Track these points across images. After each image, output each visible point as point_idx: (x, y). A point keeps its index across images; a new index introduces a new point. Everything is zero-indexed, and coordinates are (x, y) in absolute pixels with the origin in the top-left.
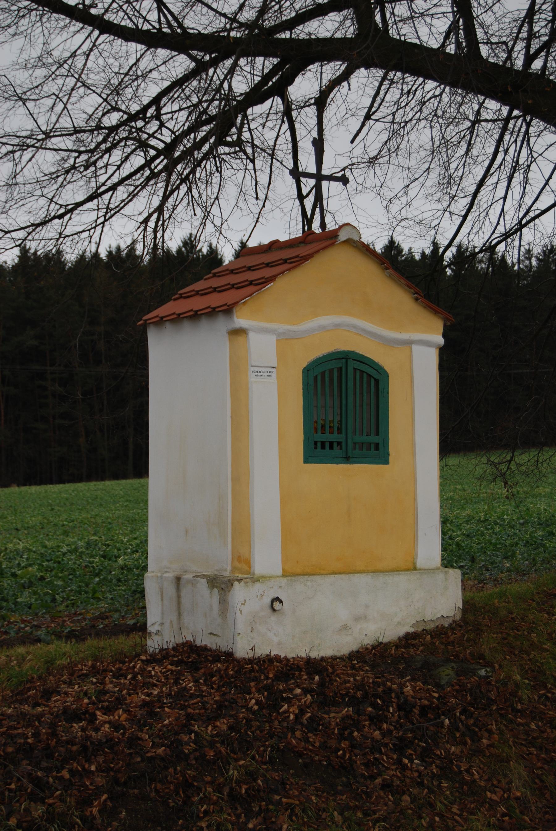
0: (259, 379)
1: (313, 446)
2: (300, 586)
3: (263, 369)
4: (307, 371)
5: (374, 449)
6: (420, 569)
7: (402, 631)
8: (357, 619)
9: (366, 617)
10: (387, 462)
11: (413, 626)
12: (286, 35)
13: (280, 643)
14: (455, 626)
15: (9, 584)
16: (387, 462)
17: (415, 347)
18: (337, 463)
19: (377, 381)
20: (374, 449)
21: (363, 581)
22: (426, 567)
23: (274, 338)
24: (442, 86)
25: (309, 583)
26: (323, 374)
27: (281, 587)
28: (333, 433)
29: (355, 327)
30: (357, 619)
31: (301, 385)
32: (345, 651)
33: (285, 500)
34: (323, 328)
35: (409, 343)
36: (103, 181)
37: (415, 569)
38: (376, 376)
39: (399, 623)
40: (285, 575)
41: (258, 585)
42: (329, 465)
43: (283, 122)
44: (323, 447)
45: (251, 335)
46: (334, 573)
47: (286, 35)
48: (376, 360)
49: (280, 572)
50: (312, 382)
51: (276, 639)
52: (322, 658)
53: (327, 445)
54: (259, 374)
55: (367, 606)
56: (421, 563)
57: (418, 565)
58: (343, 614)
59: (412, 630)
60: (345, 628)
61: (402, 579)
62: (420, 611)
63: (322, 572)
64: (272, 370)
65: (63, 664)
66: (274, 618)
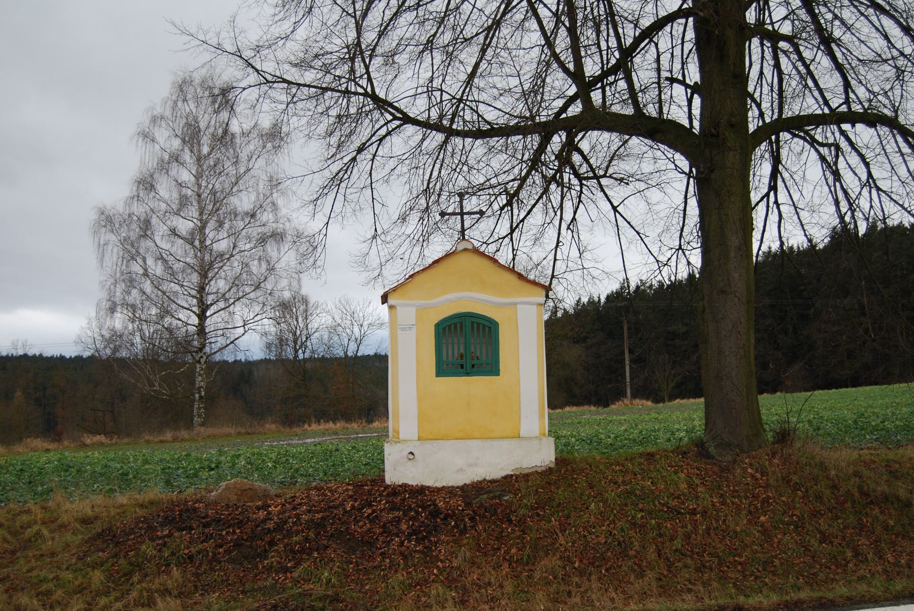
4: (437, 326)
5: (491, 367)
7: (504, 473)
8: (470, 465)
12: (564, 116)
14: (549, 471)
15: (410, 541)
19: (490, 328)
20: (491, 367)
23: (414, 309)
24: (768, 120)
26: (455, 325)
30: (470, 465)
32: (461, 484)
33: (420, 399)
35: (516, 304)
38: (488, 324)
41: (398, 445)
43: (894, 136)
45: (398, 308)
47: (564, 116)
50: (441, 331)
54: (403, 329)
57: (521, 435)
61: (505, 443)
66: (410, 463)
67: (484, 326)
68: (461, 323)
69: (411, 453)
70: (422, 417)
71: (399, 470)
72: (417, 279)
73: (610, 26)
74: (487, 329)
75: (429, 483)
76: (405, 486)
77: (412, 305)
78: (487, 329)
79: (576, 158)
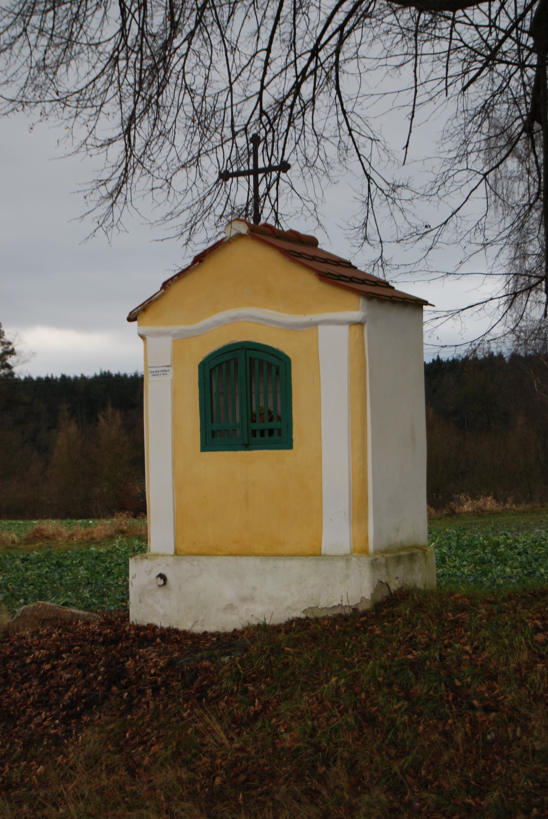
0: (156, 378)
1: (210, 435)
2: (187, 565)
3: (159, 369)
4: (203, 366)
6: (324, 555)
8: (244, 600)
9: (253, 598)
10: (290, 447)
11: (304, 611)
13: (165, 615)
16: (290, 447)
17: (320, 327)
18: (235, 450)
19: (277, 367)
21: (249, 563)
22: (332, 554)
25: (195, 563)
27: (168, 565)
28: (264, 422)
29: (252, 317)
30: (244, 600)
31: (197, 379)
34: (219, 323)
35: (315, 324)
36: (221, 214)
37: (320, 555)
39: (289, 608)
40: (176, 553)
42: (226, 453)
44: (262, 435)
46: (231, 555)
48: (275, 347)
49: (172, 552)
51: (162, 611)
52: (205, 633)
53: (258, 433)
55: (254, 588)
56: (326, 547)
57: (323, 552)
58: (229, 594)
59: (303, 616)
60: (230, 607)
61: (295, 566)
62: (314, 597)
63: (219, 553)
64: (167, 369)
65: (66, 624)
66: (160, 593)
67: (269, 365)
68: (235, 360)
69: (162, 576)
70: (181, 518)
71: (149, 607)
72: (176, 289)
73: (171, 68)
74: (265, 366)
75: (185, 625)
76: (152, 628)
77: (166, 334)
78: (265, 366)
79: (302, 105)
